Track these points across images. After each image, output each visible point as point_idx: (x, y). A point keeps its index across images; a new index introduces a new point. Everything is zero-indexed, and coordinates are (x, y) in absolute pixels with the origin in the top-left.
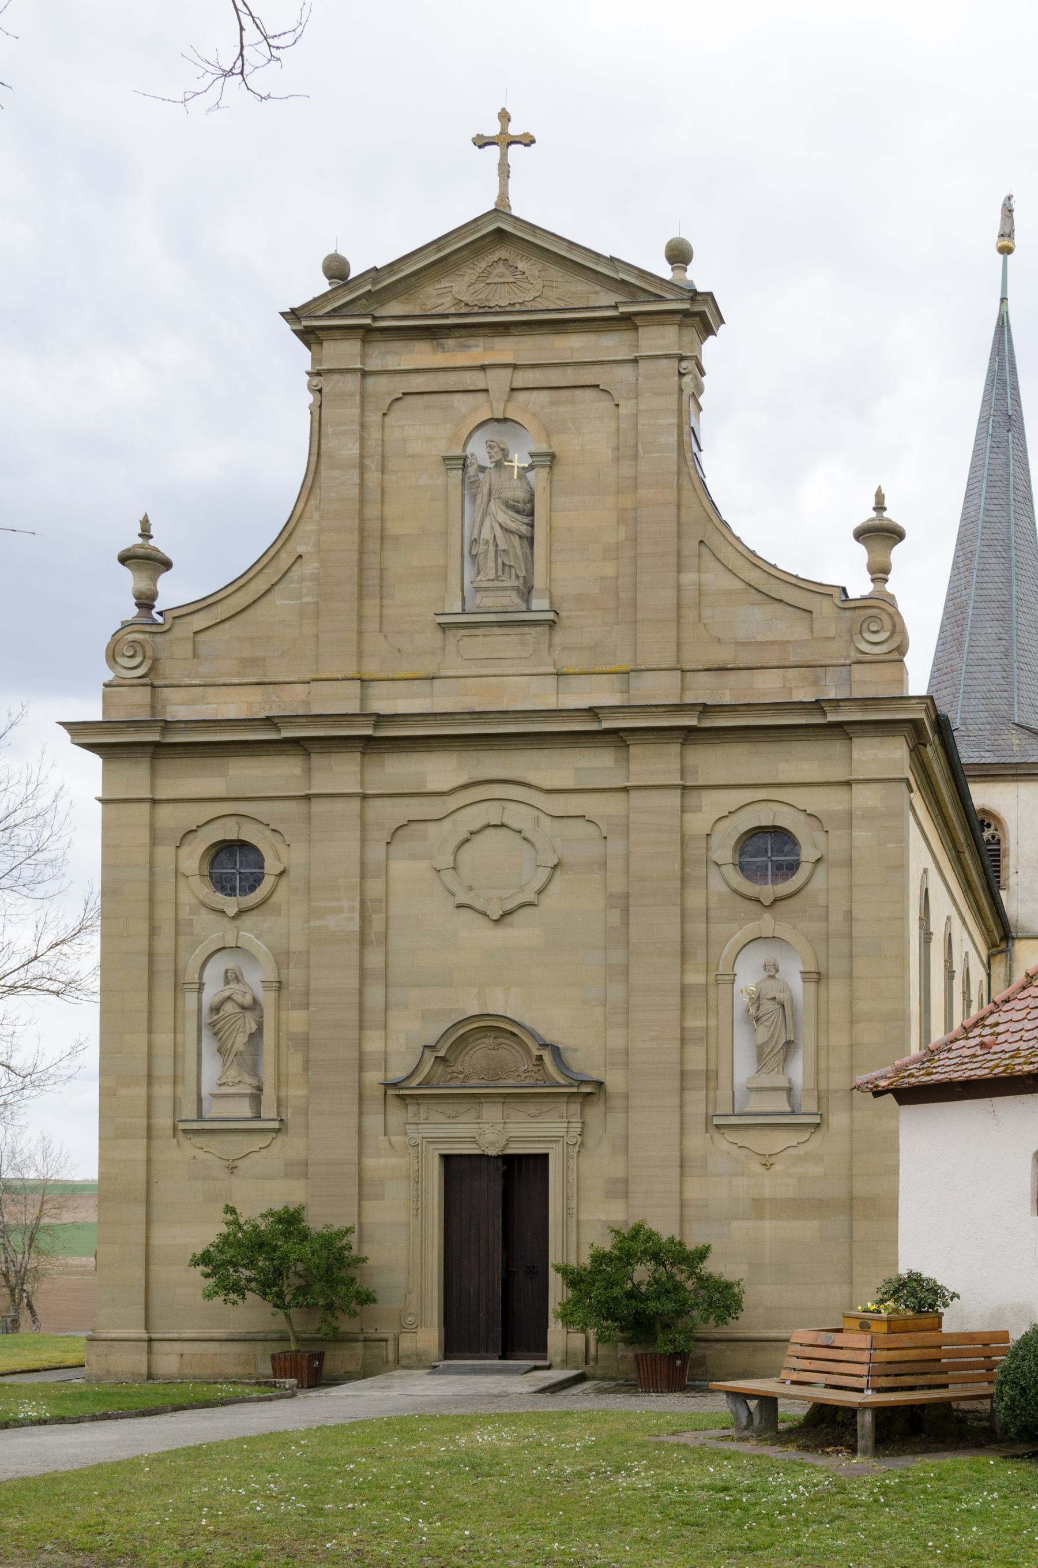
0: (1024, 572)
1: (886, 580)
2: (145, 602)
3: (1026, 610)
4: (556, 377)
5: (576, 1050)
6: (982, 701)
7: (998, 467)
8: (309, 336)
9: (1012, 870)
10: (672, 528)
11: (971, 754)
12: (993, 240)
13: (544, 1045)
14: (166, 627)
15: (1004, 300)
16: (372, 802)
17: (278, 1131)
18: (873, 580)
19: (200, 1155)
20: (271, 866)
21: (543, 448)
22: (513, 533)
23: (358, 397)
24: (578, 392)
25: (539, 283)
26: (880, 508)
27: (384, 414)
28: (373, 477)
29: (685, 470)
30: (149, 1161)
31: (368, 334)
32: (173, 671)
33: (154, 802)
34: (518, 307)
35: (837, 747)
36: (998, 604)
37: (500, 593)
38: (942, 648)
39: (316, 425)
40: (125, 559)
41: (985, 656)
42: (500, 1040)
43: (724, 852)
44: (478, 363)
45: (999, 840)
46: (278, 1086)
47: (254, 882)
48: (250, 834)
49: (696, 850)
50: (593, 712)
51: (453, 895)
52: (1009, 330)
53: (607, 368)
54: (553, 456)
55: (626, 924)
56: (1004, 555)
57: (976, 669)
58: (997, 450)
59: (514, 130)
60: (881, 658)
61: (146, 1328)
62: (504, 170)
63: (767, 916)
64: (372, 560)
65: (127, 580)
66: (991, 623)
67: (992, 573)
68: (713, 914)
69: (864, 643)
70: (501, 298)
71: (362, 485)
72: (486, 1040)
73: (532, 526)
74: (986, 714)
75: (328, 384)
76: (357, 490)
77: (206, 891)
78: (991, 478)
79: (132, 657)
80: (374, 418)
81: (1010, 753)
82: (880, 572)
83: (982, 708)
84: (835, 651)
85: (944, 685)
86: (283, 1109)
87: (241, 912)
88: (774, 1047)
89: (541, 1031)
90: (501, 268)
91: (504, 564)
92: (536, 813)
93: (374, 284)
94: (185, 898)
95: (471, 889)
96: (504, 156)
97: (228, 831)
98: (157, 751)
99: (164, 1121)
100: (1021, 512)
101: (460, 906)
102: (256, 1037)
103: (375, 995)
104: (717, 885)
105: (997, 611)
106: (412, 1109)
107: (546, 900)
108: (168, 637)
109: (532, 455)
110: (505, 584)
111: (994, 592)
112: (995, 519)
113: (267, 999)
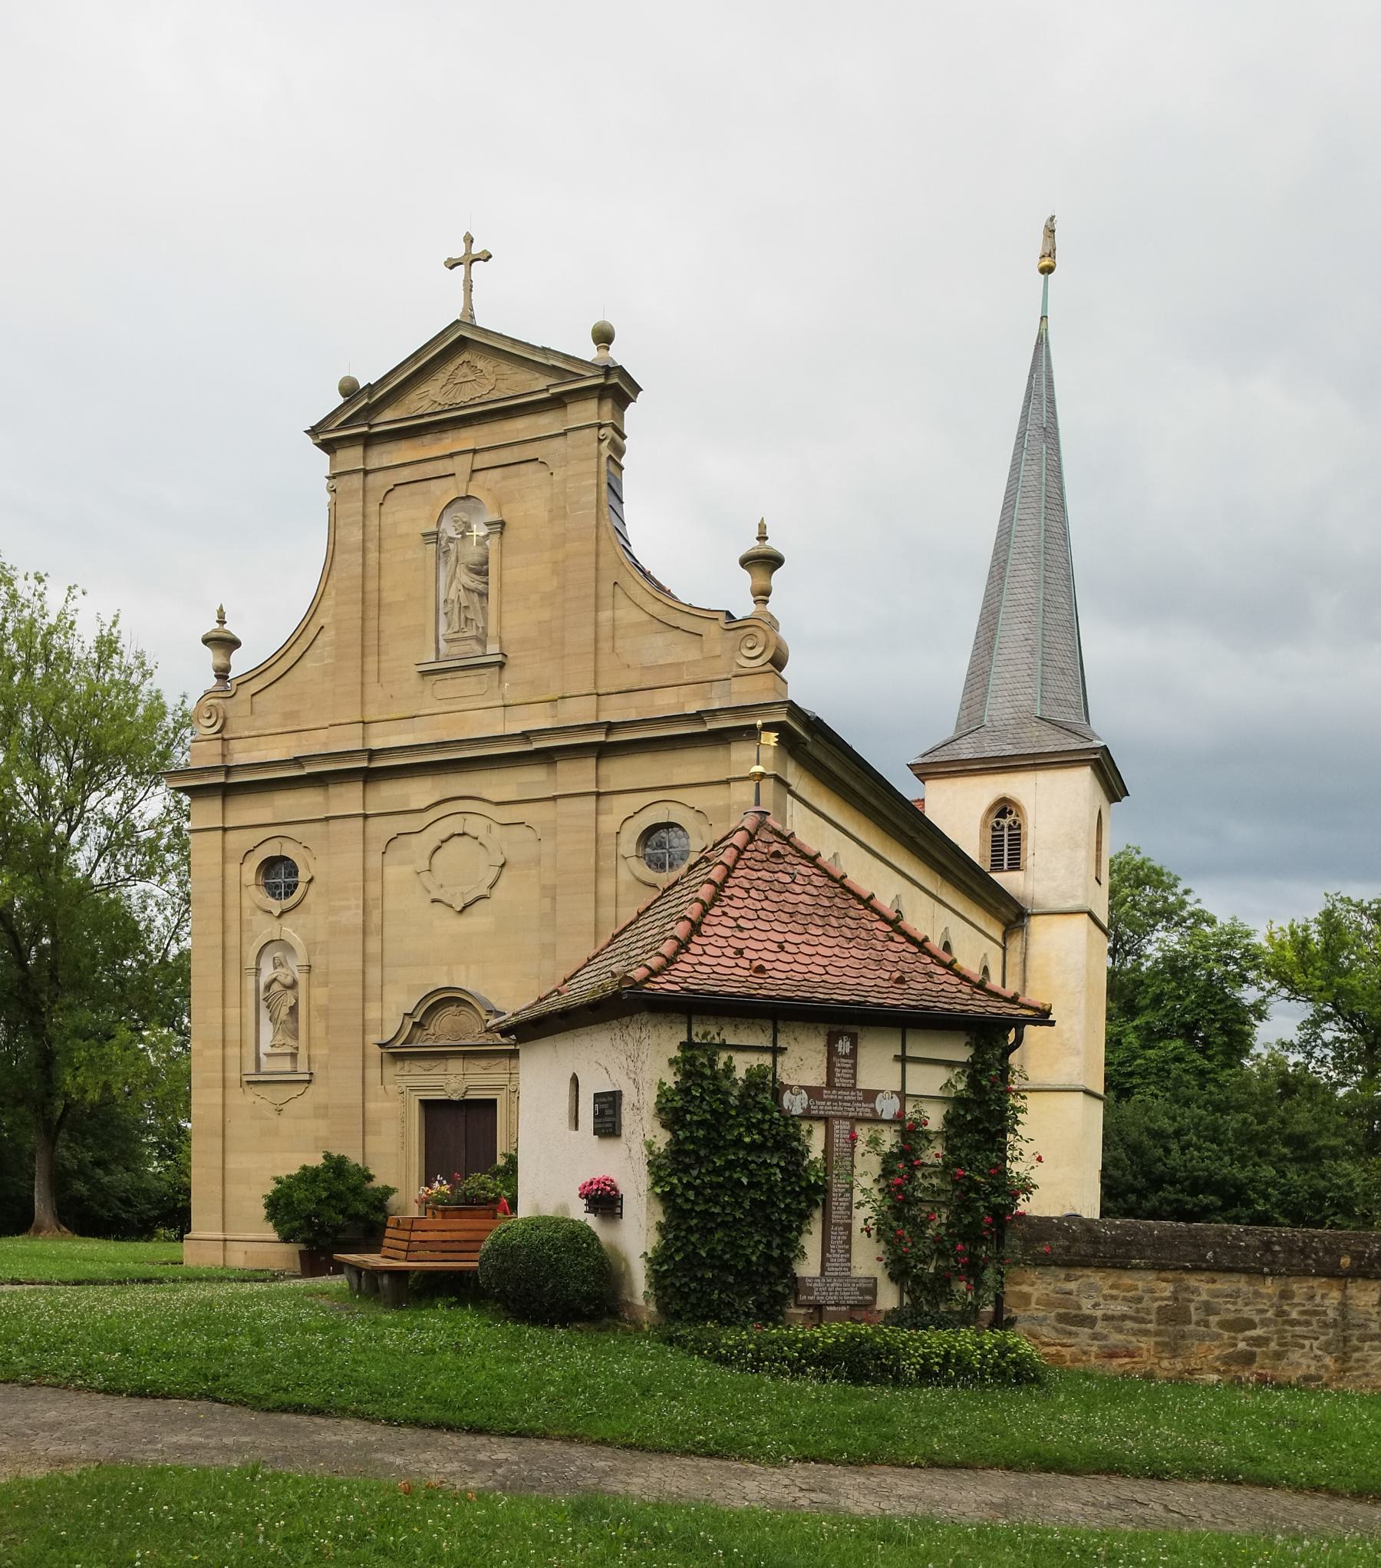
0: (1053, 575)
1: (766, 602)
2: (222, 673)
3: (1053, 610)
4: (506, 456)
6: (1009, 699)
7: (1032, 478)
8: (328, 446)
9: (1030, 852)
10: (592, 573)
11: (994, 748)
12: (1036, 263)
14: (232, 693)
15: (1044, 318)
16: (371, 820)
17: (309, 1082)
18: (755, 602)
19: (258, 1100)
20: (303, 876)
21: (496, 517)
22: (473, 591)
23: (361, 492)
24: (522, 466)
25: (493, 378)
26: (762, 538)
27: (381, 504)
28: (372, 556)
29: (603, 523)
30: (224, 1105)
31: (368, 441)
32: (236, 728)
33: (225, 830)
34: (477, 401)
35: (719, 753)
37: (463, 643)
38: (976, 652)
39: (332, 519)
40: (206, 641)
41: (1013, 656)
42: (461, 1008)
43: (629, 844)
44: (448, 453)
45: (1020, 825)
46: (309, 1047)
47: (291, 888)
48: (290, 851)
49: (607, 847)
50: (526, 736)
51: (429, 892)
52: (1047, 346)
53: (544, 442)
54: (503, 524)
55: (554, 909)
56: (1034, 560)
57: (1003, 669)
58: (1030, 462)
59: (476, 250)
60: (757, 670)
61: (224, 1231)
62: (468, 287)
64: (372, 624)
65: (209, 657)
66: (1020, 626)
67: (1023, 579)
68: (620, 899)
69: (743, 658)
70: (463, 398)
71: (364, 565)
72: (451, 1008)
73: (487, 583)
74: (1012, 710)
75: (340, 484)
76: (360, 569)
77: (261, 897)
78: (1024, 490)
79: (209, 718)
80: (373, 508)
81: (1028, 745)
82: (762, 595)
83: (1008, 704)
84: (720, 668)
85: (975, 686)
86: (312, 1065)
87: (282, 913)
90: (465, 369)
91: (467, 619)
92: (489, 822)
93: (370, 398)
94: (246, 903)
95: (442, 886)
96: (468, 272)
98: (227, 791)
99: (234, 1075)
100: (1052, 518)
101: (433, 901)
102: (293, 1010)
103: (374, 973)
104: (624, 875)
105: (1026, 613)
106: (399, 1065)
108: (233, 700)
109: (487, 524)
110: (466, 635)
111: (1023, 596)
112: (1027, 528)
113: (302, 979)
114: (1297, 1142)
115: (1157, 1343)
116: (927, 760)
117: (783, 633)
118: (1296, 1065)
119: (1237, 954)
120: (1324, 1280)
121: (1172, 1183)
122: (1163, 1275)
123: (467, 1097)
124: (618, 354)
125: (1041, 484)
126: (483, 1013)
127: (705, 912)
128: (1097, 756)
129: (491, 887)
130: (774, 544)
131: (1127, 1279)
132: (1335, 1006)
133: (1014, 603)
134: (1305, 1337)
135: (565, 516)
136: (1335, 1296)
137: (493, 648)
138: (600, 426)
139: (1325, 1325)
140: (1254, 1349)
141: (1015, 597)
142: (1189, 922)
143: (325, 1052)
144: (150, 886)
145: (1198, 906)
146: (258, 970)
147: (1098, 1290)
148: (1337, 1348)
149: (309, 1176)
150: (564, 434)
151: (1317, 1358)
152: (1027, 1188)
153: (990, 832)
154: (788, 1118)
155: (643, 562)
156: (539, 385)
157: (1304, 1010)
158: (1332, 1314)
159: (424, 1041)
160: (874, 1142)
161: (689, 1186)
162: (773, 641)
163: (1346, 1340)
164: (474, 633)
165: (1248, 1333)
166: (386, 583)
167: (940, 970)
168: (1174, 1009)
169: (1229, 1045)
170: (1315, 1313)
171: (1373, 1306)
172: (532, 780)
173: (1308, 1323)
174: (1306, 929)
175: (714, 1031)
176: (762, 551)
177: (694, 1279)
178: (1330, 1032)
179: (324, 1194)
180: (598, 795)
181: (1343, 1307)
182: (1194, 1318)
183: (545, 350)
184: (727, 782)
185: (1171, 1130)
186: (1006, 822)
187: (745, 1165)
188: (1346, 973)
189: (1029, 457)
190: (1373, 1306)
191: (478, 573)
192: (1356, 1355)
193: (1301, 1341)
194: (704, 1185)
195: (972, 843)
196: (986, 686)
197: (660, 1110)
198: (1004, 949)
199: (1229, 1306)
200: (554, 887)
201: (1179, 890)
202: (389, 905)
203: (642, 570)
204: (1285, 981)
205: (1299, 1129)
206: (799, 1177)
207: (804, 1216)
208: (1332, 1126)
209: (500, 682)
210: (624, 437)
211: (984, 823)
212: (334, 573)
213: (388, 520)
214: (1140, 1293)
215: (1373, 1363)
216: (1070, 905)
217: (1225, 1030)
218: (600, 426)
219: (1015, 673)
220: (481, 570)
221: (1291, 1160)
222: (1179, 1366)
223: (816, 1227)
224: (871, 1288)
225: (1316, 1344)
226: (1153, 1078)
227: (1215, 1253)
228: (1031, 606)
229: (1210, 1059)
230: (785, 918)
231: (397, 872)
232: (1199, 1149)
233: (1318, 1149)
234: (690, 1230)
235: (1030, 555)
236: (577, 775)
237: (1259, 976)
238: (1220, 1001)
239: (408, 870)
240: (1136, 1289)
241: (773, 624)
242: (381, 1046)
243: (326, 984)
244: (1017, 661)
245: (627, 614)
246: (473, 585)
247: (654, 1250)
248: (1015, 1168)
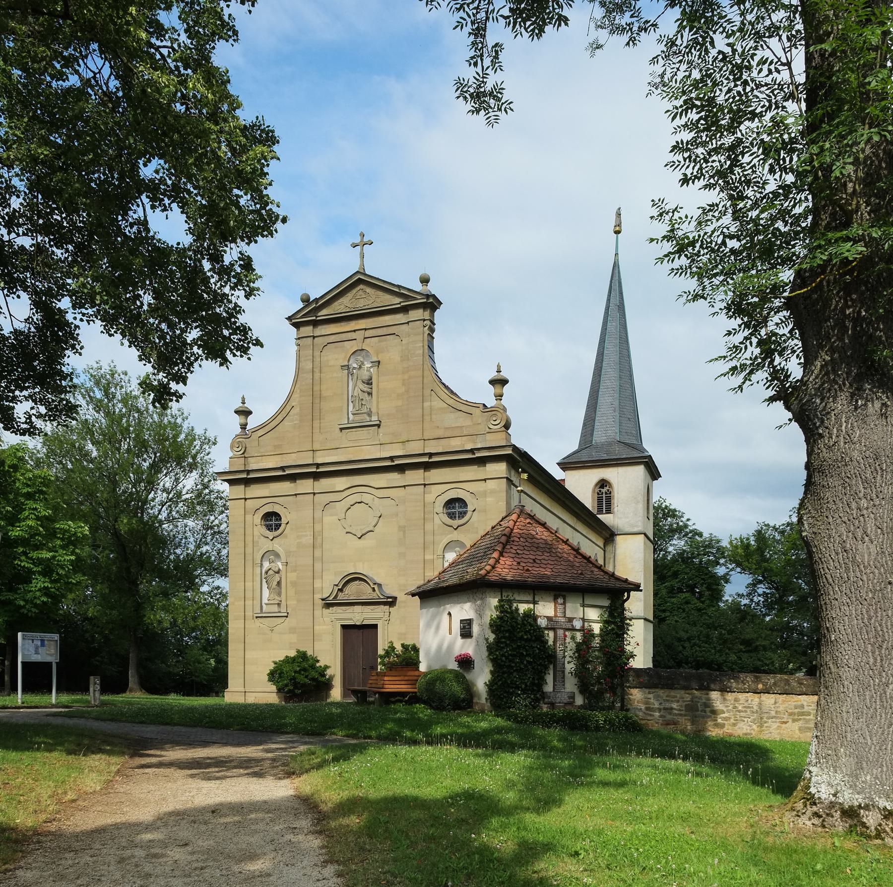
2: (244, 427)
8: (297, 325)
13: (375, 584)
15: (616, 254)
20: (284, 521)
21: (375, 359)
25: (374, 297)
26: (499, 371)
28: (317, 375)
31: (315, 324)
43: (439, 507)
47: (278, 527)
48: (277, 509)
50: (392, 458)
59: (366, 239)
62: (362, 256)
63: (455, 532)
64: (316, 406)
65: (238, 420)
80: (317, 353)
82: (499, 397)
84: (483, 429)
89: (375, 578)
90: (361, 293)
94: (256, 533)
97: (268, 509)
98: (247, 482)
99: (249, 613)
102: (279, 583)
103: (318, 566)
107: (377, 529)
114: (747, 643)
116: (565, 461)
117: (509, 413)
118: (745, 605)
119: (714, 551)
121: (687, 664)
124: (433, 288)
126: (371, 584)
127: (504, 548)
130: (504, 374)
131: (673, 693)
132: (763, 576)
135: (408, 359)
136: (757, 700)
137: (374, 418)
138: (424, 320)
142: (690, 535)
143: (295, 602)
144: (190, 523)
145: (694, 527)
146: (262, 564)
147: (661, 697)
149: (288, 660)
150: (408, 323)
151: (750, 726)
152: (632, 656)
153: (596, 496)
154: (539, 628)
155: (443, 381)
156: (396, 301)
157: (747, 579)
160: (573, 638)
161: (503, 655)
162: (505, 418)
163: (761, 718)
164: (365, 411)
166: (324, 387)
167: (596, 570)
168: (684, 578)
169: (712, 595)
172: (394, 478)
173: (746, 711)
174: (748, 539)
175: (511, 594)
176: (499, 378)
177: (505, 692)
178: (761, 589)
179: (298, 669)
180: (425, 485)
183: (399, 287)
184: (485, 480)
185: (685, 637)
186: (604, 490)
187: (524, 647)
188: (767, 560)
191: (368, 384)
194: (509, 655)
195: (587, 498)
197: (491, 626)
198: (605, 551)
200: (405, 527)
201: (684, 519)
202: (326, 534)
203: (443, 384)
204: (739, 564)
205: (748, 637)
206: (545, 652)
207: (547, 668)
208: (763, 635)
210: (434, 324)
211: (594, 491)
212: (299, 382)
213: (324, 359)
216: (635, 530)
217: (709, 588)
218: (424, 320)
220: (369, 382)
221: (744, 652)
223: (551, 672)
224: (572, 697)
226: (675, 613)
229: (703, 602)
230: (535, 549)
231: (329, 519)
232: (700, 647)
233: (757, 646)
234: (504, 673)
237: (726, 562)
238: (706, 574)
239: (335, 518)
241: (505, 409)
242: (323, 600)
243: (295, 571)
245: (437, 404)
246: (365, 389)
248: (628, 648)
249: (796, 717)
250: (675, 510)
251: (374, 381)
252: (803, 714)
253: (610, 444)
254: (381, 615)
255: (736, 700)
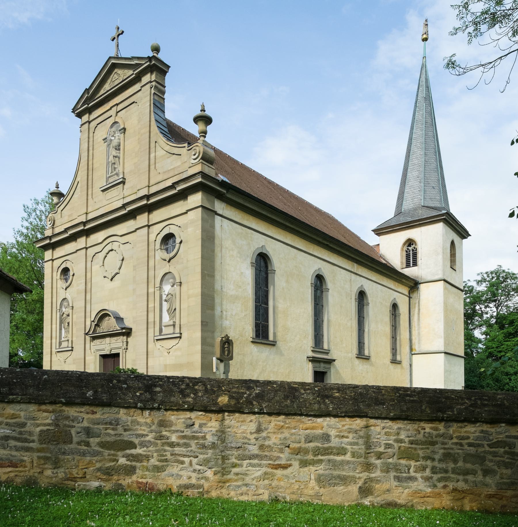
5: (127, 318)
6: (411, 201)
8: (80, 115)
36: (418, 165)
41: (413, 185)
45: (416, 249)
56: (421, 147)
58: (419, 111)
72: (107, 318)
88: (171, 310)
90: (115, 75)
100: (428, 130)
104: (158, 257)
105: (418, 168)
115: (39, 458)
120: (201, 413)
122: (44, 407)
123: (112, 353)
125: (423, 118)
128: (444, 217)
129: (120, 269)
133: (413, 164)
134: (184, 456)
139: (204, 447)
140: (134, 463)
141: (413, 162)
148: (216, 463)
153: (405, 253)
158: (210, 439)
159: (101, 330)
165: (128, 452)
170: (194, 438)
171: (251, 433)
173: (187, 445)
181: (222, 434)
182: (75, 439)
186: (410, 248)
189: (419, 109)
190: (251, 433)
192: (235, 470)
193: (182, 459)
196: (403, 198)
198: (410, 298)
199: (110, 431)
209: (123, 189)
214: (23, 420)
215: (253, 477)
219: (414, 191)
222: (61, 475)
225: (195, 461)
227: (96, 392)
228: (420, 165)
235: (419, 145)
236: (142, 219)
239: (98, 266)
240: (20, 417)
244: (414, 186)
247: (215, 414)
249: (310, 457)
250: (514, 274)
251: (122, 147)
252: (327, 451)
253: (415, 209)
254: (120, 345)
255: (163, 424)
